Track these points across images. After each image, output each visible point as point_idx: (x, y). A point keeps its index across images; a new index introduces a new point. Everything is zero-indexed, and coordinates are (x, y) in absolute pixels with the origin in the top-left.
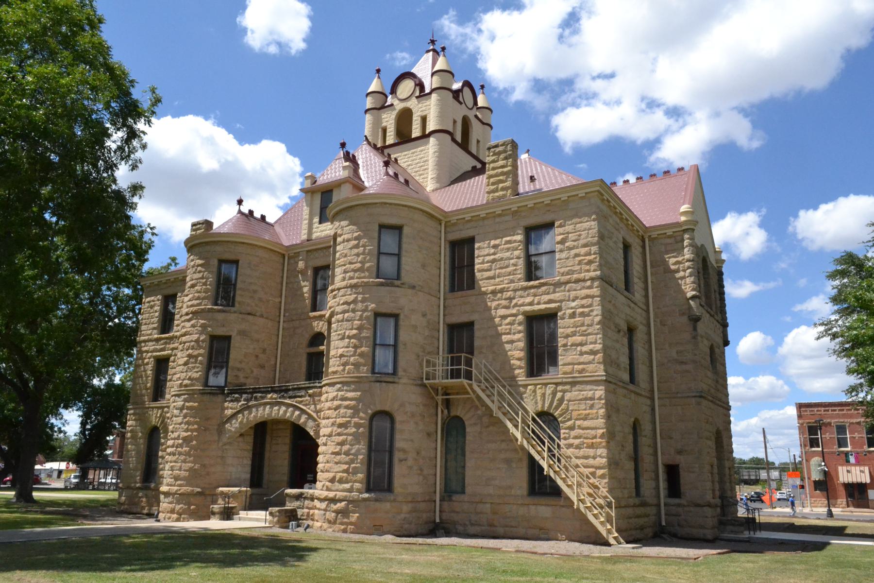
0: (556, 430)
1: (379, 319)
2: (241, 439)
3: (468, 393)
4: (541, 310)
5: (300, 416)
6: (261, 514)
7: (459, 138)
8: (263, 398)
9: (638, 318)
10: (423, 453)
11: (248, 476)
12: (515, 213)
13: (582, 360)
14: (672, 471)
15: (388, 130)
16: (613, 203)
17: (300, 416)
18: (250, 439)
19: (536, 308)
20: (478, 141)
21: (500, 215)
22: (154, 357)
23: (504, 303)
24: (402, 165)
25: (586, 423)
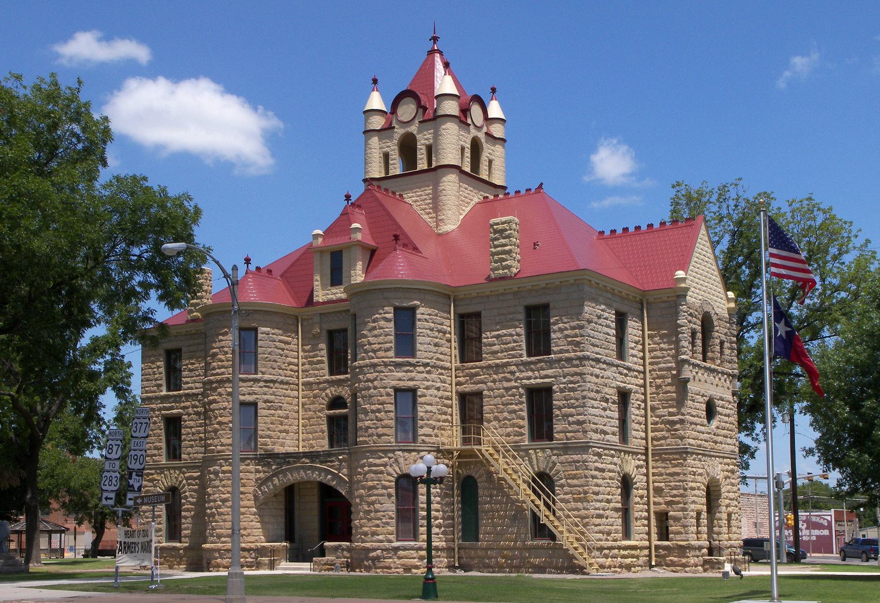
0: (552, 488)
1: (398, 394)
2: (274, 499)
3: (477, 457)
4: (538, 384)
5: (422, 509)
6: (307, 565)
7: (467, 169)
8: (295, 462)
9: (632, 383)
10: (87, 470)
11: (283, 532)
12: (515, 294)
13: (570, 429)
14: (663, 518)
15: (391, 157)
16: (602, 284)
17: (422, 509)
18: (282, 499)
19: (532, 381)
20: (490, 162)
21: (503, 294)
22: (163, 415)
23: (508, 375)
24: (407, 200)
25: (575, 482)
